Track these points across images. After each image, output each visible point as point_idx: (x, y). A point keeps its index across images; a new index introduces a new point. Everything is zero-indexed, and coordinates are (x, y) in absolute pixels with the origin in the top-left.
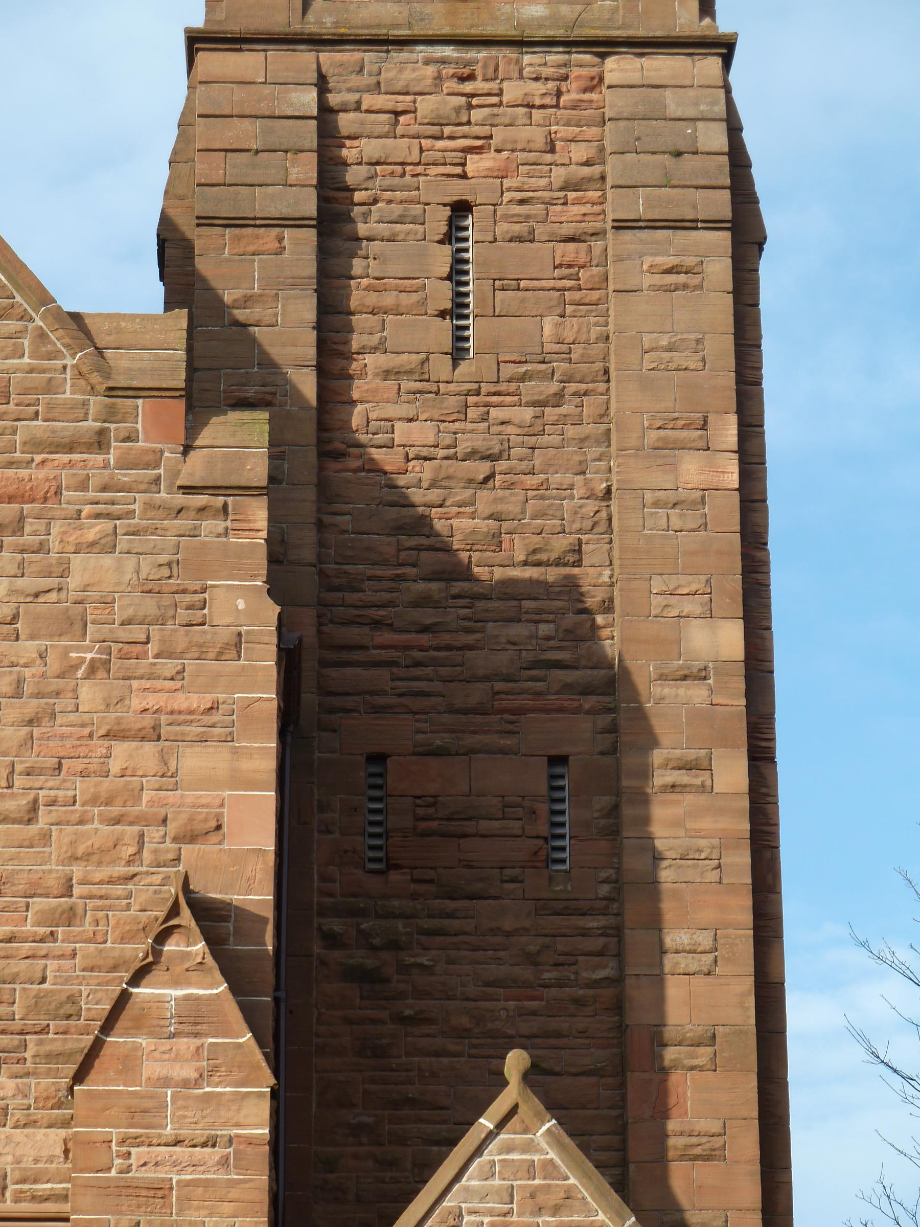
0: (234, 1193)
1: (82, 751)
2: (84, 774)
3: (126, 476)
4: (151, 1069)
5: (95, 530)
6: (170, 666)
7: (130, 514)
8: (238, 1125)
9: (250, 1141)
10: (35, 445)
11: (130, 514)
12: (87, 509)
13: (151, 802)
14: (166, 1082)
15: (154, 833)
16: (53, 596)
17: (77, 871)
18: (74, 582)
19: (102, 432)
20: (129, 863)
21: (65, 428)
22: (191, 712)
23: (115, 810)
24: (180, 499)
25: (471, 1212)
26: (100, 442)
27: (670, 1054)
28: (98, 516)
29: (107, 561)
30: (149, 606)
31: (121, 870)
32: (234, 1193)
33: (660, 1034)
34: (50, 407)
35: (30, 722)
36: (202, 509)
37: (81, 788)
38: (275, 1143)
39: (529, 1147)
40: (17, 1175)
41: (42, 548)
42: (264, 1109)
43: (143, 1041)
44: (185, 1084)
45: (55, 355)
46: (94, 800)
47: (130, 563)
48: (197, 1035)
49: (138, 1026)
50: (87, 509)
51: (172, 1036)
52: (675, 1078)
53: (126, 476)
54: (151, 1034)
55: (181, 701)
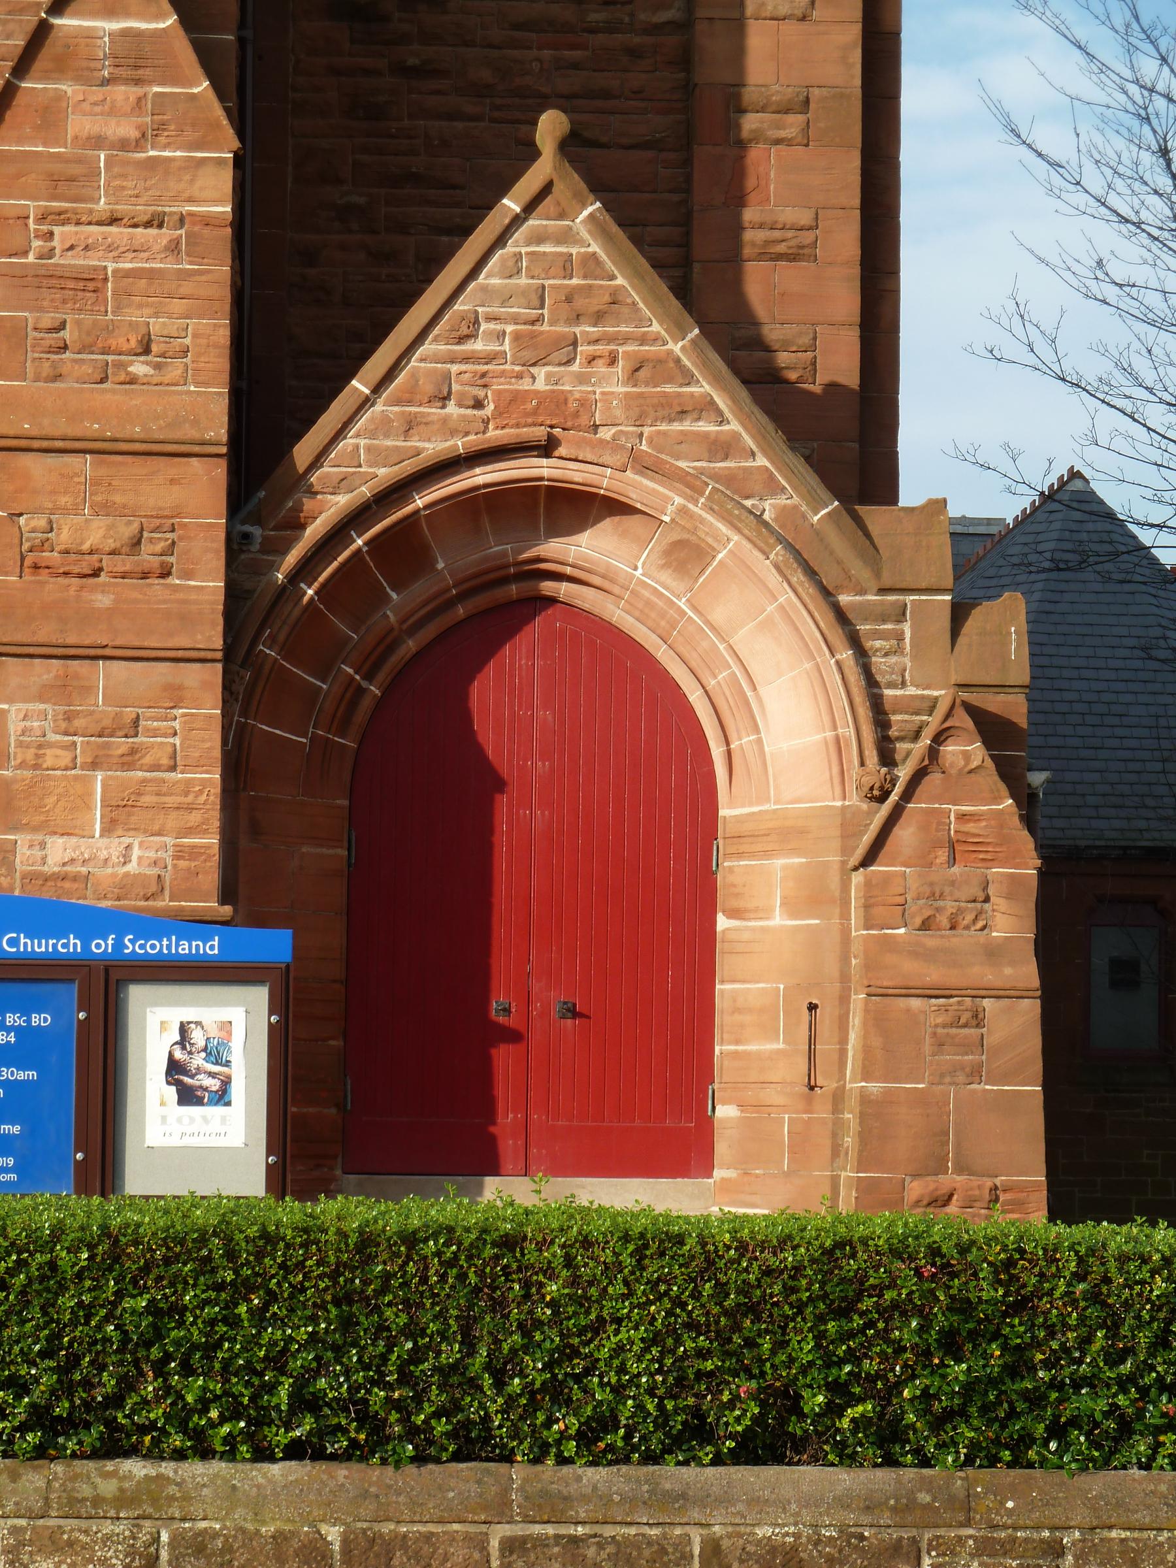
0: (187, 288)
4: (78, 125)
8: (191, 200)
9: (207, 221)
14: (98, 142)
25: (489, 319)
27: (750, 123)
32: (187, 288)
33: (738, 96)
38: (239, 223)
39: (566, 237)
42: (225, 180)
43: (68, 88)
44: (124, 145)
48: (138, 82)
49: (61, 69)
51: (106, 82)
52: (755, 154)
54: (79, 79)
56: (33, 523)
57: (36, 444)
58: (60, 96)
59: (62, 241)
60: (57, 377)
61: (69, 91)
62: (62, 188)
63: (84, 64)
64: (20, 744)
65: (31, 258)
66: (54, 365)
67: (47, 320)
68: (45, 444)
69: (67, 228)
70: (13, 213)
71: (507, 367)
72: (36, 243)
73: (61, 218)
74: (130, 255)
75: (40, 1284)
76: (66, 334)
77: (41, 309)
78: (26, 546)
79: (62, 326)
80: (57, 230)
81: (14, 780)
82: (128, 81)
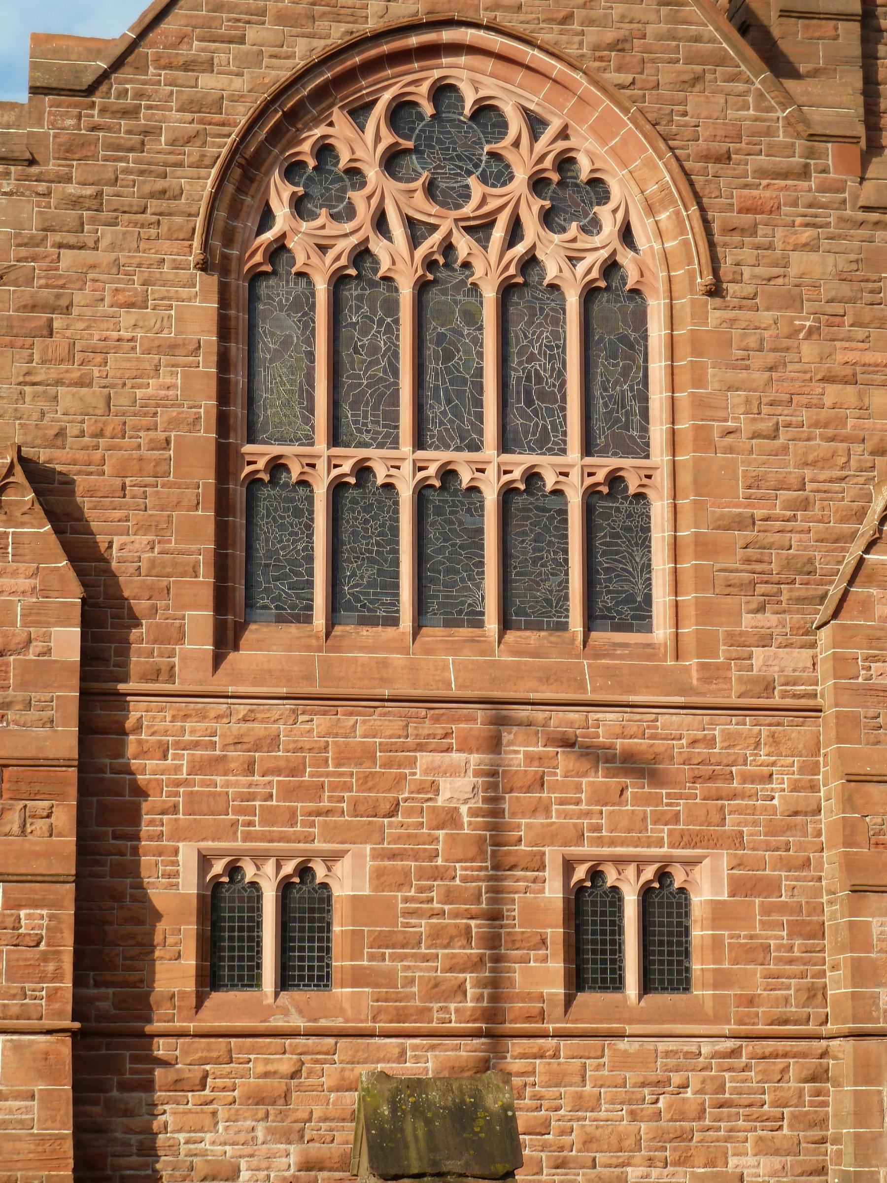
1: (806, 390)
2: (808, 406)
3: (824, 198)
5: (806, 235)
6: (861, 333)
7: (827, 225)
10: (762, 173)
11: (827, 225)
12: (799, 220)
13: (854, 427)
15: (857, 448)
16: (780, 281)
17: (808, 473)
18: (793, 271)
19: (807, 166)
20: (842, 468)
21: (780, 162)
22: (877, 365)
23: (830, 432)
24: (861, 215)
26: (804, 173)
28: (807, 225)
29: (815, 257)
30: (845, 289)
31: (836, 473)
34: (770, 146)
35: (771, 369)
36: (876, 223)
37: (805, 415)
40: (782, 680)
41: (770, 247)
43: (874, 591)
45: (770, 109)
46: (816, 425)
47: (831, 258)
49: (871, 580)
50: (799, 220)
53: (824, 198)
54: (880, 587)
55: (870, 357)
56: (875, 820)
57: (875, 779)
58: (871, 596)
59: (876, 671)
60: (878, 743)
61: (875, 592)
62: (874, 643)
63: (882, 578)
64: (879, 940)
65: (860, 680)
66: (876, 736)
67: (871, 712)
68: (880, 778)
69: (878, 664)
70: (851, 656)
71: (280, 753)
72: (863, 672)
73: (875, 659)
74: (232, 748)
75: (669, 1079)
76: (880, 720)
77: (867, 707)
78: (872, 833)
79: (878, 716)
80: (872, 665)
81: (877, 959)
82: (798, 612)
